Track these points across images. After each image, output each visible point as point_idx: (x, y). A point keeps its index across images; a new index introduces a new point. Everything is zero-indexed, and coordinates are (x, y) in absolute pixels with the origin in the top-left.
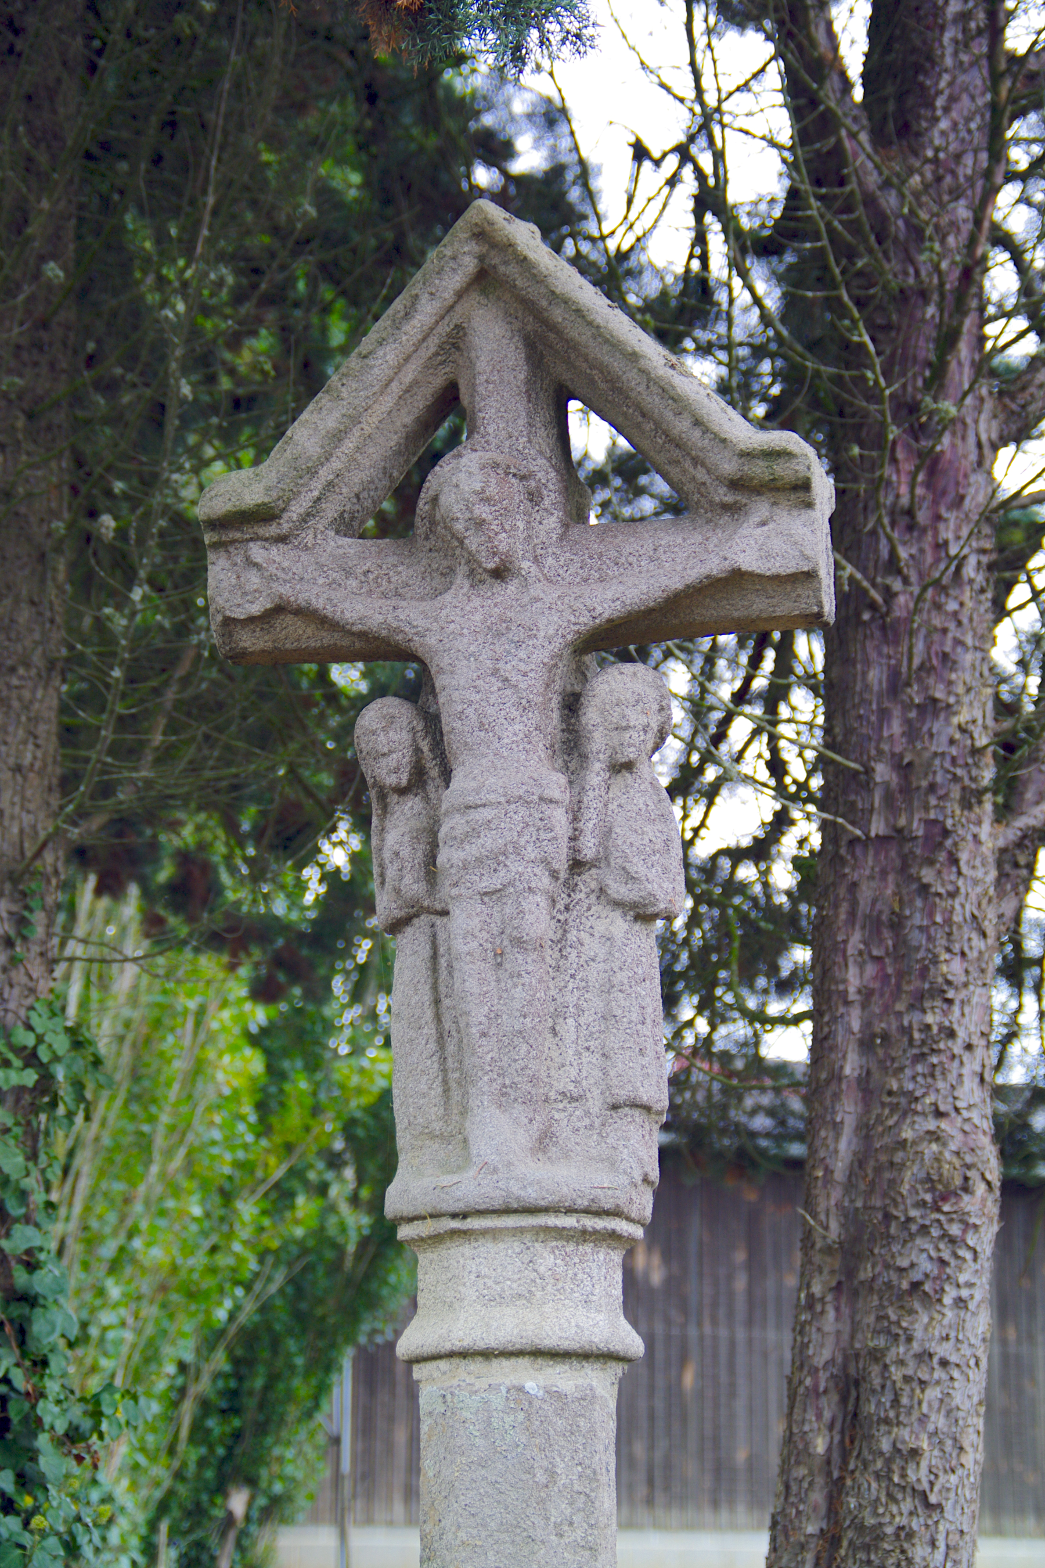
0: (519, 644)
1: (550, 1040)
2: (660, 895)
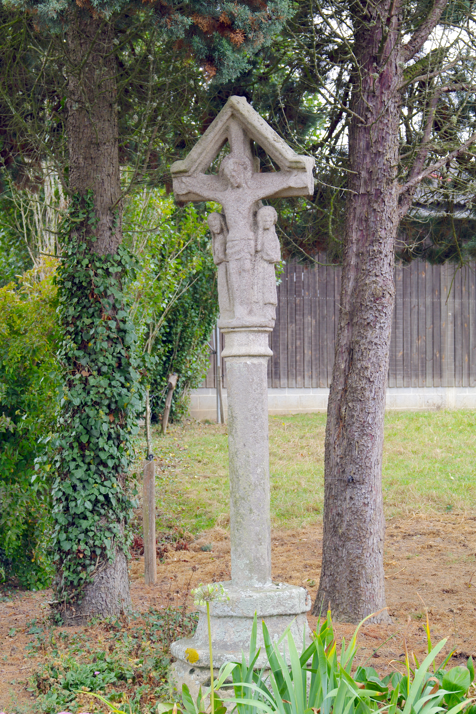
0: (242, 204)
1: (251, 290)
2: (274, 258)
